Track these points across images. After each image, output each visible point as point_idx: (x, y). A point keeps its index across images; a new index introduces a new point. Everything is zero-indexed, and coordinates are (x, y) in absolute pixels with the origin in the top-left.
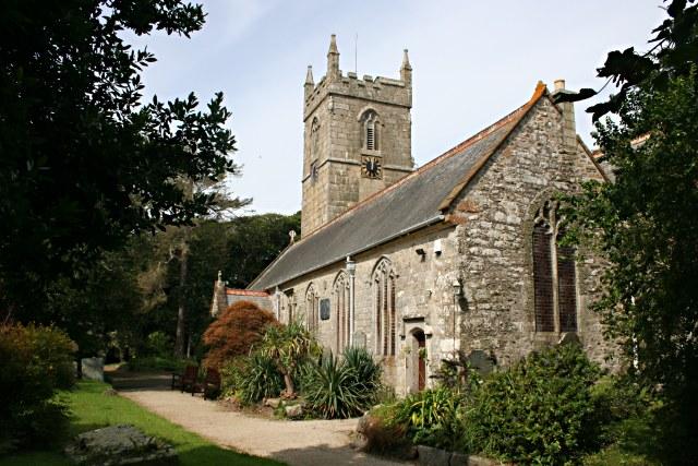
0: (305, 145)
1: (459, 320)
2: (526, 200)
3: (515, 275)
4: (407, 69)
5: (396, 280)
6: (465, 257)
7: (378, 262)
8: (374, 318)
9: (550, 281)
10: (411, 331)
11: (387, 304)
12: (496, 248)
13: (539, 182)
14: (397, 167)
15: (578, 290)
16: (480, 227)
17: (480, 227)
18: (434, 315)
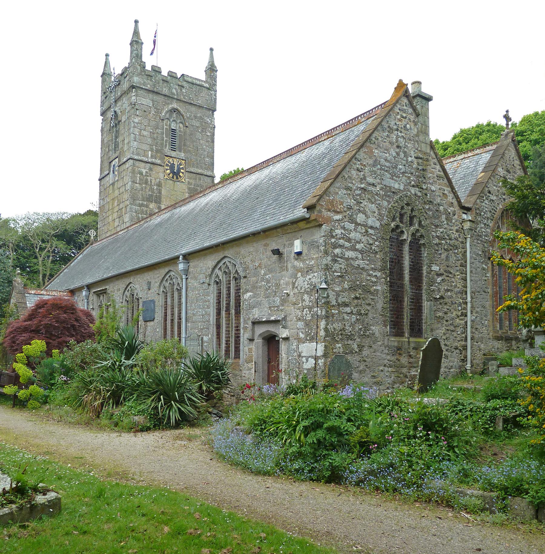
0: (102, 141)
1: (323, 324)
2: (385, 203)
3: (374, 279)
4: (211, 69)
5: (243, 281)
6: (329, 258)
7: (219, 262)
8: (212, 319)
9: (402, 286)
10: (260, 335)
11: (229, 306)
12: (357, 250)
13: (397, 186)
14: (200, 171)
15: (424, 297)
16: (344, 228)
17: (344, 228)
18: (292, 318)
